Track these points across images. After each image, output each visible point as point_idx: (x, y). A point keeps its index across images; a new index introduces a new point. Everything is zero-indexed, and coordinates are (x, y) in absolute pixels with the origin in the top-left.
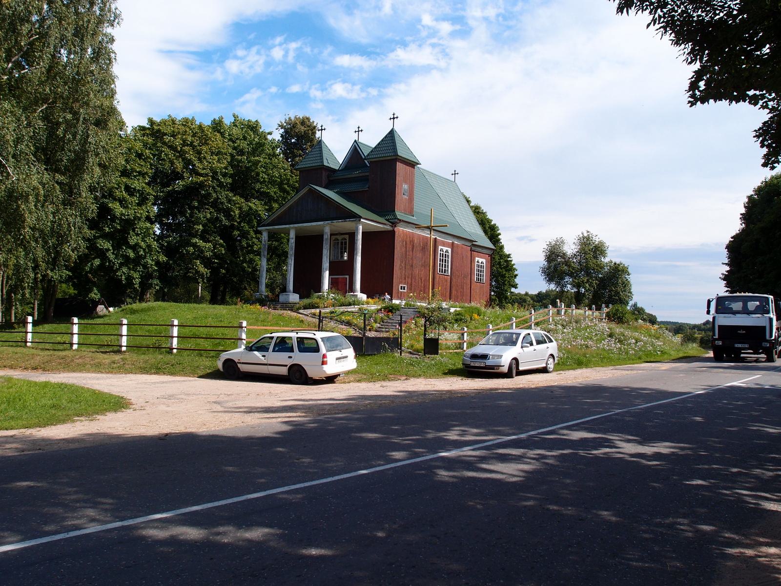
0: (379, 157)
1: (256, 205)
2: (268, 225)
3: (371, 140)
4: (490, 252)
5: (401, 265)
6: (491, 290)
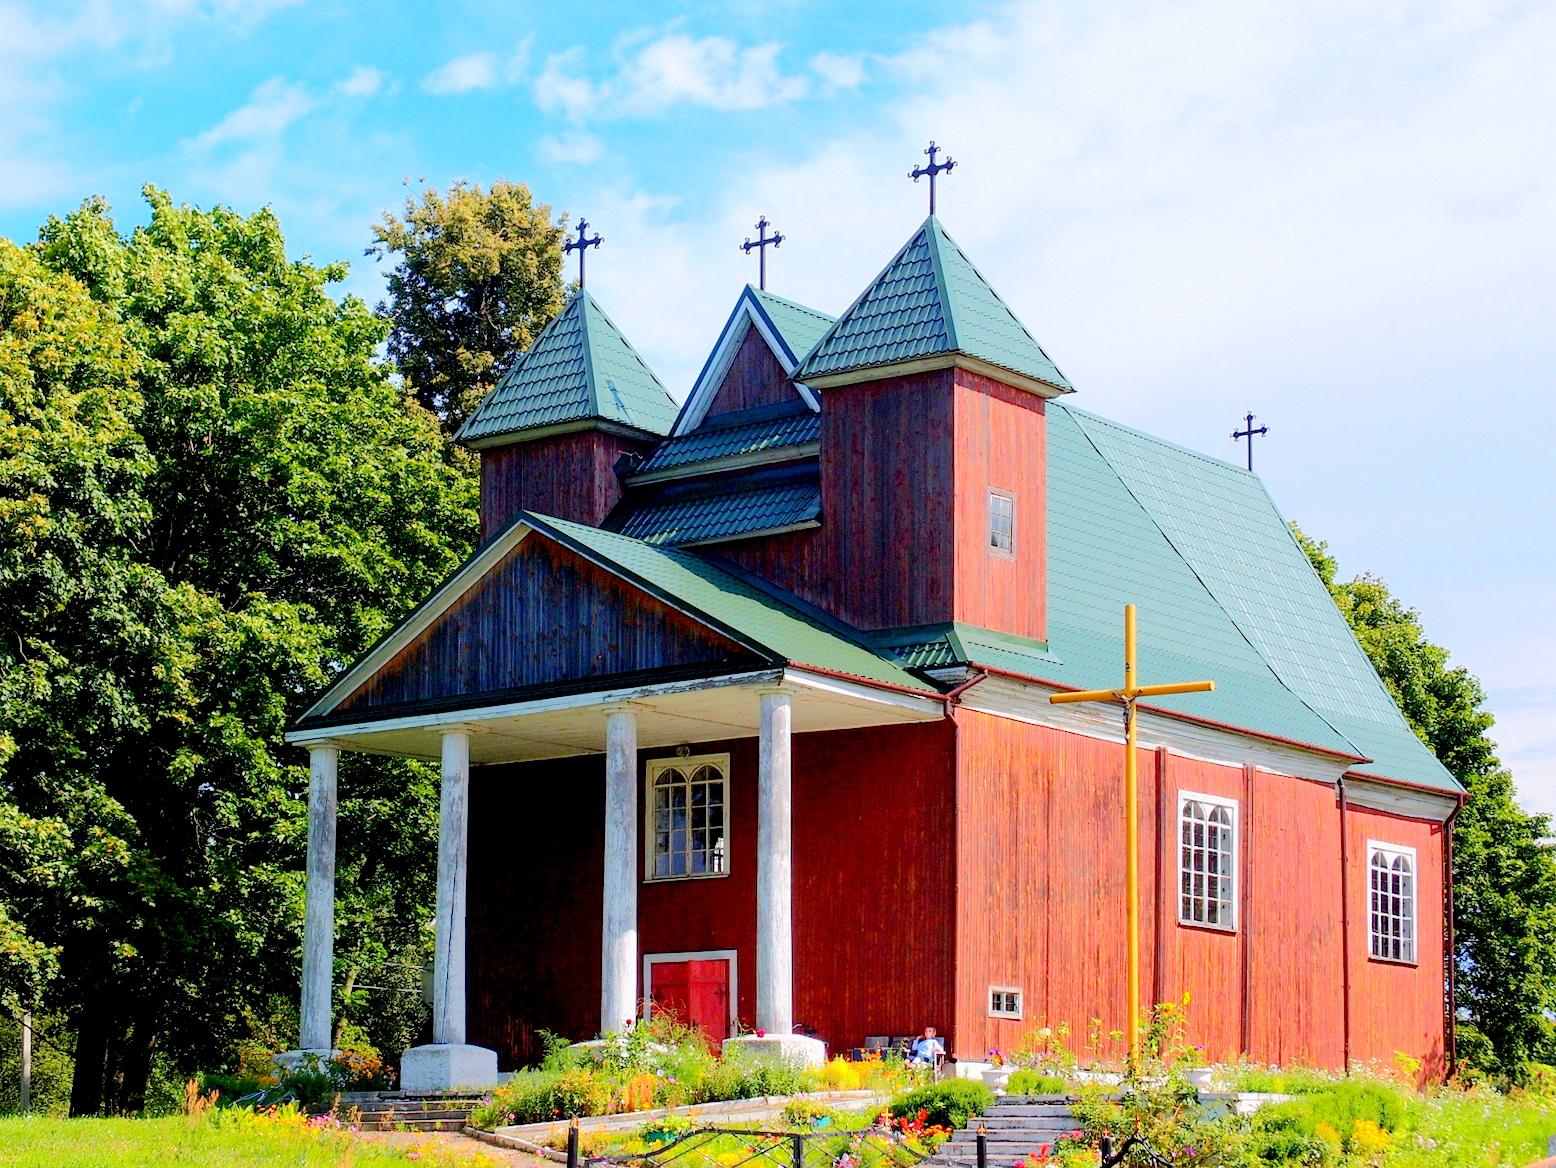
0: (864, 367)
1: (282, 625)
2: (338, 717)
3: (820, 287)
4: (1441, 810)
5: (990, 891)
6: (1452, 1003)
